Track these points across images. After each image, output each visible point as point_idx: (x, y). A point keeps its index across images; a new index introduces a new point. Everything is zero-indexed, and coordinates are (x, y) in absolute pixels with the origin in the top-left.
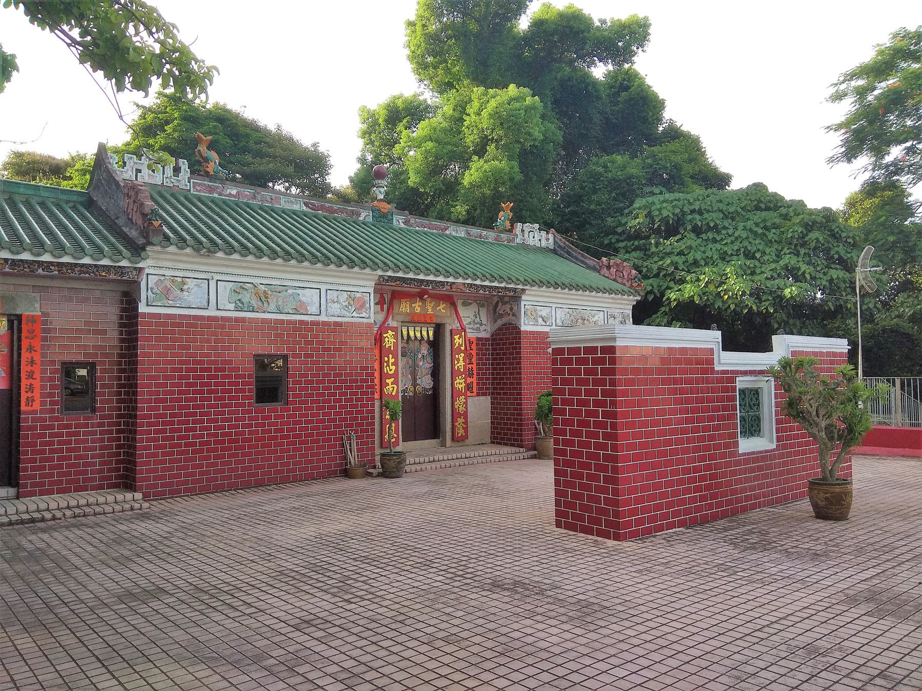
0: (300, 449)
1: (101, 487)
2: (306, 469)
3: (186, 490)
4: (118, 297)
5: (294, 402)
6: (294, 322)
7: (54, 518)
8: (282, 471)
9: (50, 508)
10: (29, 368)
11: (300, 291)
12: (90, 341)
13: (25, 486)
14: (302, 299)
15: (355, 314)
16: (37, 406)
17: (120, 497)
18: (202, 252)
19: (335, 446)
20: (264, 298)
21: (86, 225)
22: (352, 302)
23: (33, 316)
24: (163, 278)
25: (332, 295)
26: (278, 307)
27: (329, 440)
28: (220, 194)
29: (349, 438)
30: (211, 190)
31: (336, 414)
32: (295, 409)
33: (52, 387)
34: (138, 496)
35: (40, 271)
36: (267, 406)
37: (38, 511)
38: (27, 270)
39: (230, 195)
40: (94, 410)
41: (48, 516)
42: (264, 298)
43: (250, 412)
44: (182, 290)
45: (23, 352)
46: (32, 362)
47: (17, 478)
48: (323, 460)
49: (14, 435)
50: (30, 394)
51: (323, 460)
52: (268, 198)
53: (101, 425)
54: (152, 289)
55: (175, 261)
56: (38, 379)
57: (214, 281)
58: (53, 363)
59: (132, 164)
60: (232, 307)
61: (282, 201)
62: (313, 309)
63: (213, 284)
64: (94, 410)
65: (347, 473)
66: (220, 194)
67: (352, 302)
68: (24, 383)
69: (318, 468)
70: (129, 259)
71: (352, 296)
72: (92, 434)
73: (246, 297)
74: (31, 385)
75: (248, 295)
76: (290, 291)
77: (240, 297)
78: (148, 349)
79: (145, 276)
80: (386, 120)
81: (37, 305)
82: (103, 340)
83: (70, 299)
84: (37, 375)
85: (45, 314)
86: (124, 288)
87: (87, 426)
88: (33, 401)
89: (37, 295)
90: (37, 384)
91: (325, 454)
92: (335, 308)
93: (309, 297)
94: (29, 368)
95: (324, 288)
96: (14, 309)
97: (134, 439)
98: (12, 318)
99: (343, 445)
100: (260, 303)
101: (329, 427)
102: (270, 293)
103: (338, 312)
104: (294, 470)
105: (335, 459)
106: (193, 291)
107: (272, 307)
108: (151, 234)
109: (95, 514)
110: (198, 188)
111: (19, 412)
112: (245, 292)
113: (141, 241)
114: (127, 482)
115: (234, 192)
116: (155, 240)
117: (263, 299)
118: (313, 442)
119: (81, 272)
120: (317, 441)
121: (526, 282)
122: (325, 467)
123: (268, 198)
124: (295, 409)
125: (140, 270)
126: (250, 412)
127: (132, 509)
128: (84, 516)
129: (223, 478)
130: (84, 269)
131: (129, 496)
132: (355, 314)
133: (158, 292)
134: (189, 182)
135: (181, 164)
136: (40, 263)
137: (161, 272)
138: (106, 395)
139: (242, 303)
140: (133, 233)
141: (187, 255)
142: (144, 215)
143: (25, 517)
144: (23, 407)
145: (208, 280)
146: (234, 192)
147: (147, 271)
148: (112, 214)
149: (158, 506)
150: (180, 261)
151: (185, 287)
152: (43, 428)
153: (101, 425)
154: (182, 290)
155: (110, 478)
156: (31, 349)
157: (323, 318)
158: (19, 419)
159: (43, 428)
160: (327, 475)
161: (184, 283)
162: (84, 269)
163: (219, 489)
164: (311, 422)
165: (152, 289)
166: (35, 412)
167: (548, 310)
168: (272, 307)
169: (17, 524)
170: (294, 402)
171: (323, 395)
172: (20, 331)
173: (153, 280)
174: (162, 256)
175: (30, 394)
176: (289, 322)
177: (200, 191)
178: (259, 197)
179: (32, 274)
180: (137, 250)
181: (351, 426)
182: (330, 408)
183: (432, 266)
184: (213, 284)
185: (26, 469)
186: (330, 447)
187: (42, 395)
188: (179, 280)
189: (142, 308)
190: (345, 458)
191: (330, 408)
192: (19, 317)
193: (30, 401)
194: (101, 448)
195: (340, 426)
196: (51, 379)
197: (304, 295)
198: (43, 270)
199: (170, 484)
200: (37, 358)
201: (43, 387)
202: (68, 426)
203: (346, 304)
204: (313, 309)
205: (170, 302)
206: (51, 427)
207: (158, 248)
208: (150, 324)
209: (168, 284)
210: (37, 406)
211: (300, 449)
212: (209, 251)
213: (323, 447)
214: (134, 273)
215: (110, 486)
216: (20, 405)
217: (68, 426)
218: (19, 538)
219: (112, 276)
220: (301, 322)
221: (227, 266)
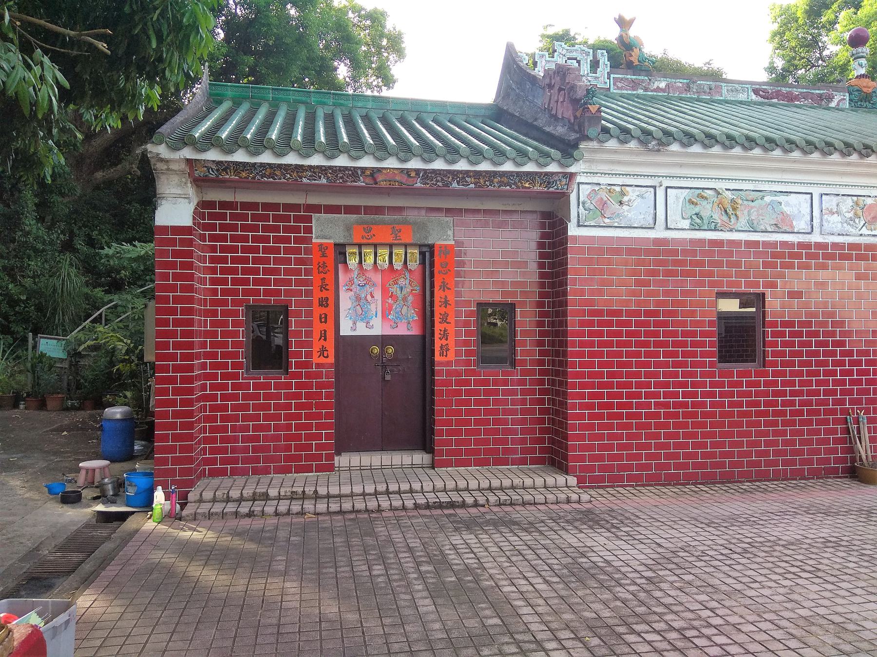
0: (784, 433)
1: (523, 462)
2: (793, 462)
3: (630, 478)
4: (535, 219)
5: (774, 364)
6: (774, 244)
7: (476, 505)
8: (757, 464)
9: (471, 487)
10: (443, 310)
11: (781, 198)
12: (509, 275)
13: (441, 453)
14: (785, 209)
15: (864, 231)
16: (451, 356)
17: (550, 481)
18: (650, 146)
19: (834, 431)
20: (730, 210)
21: (502, 136)
22: (860, 212)
23: (446, 246)
24: (597, 188)
25: (830, 203)
26: (751, 223)
27: (826, 422)
28: (646, 90)
29: (857, 421)
30: (635, 85)
31: (836, 383)
32: (776, 374)
33: (467, 333)
34: (572, 480)
35: (455, 185)
36: (736, 368)
37: (457, 490)
38: (440, 184)
39: (658, 89)
40: (514, 363)
41: (470, 500)
42: (730, 210)
43: (712, 375)
44: (621, 203)
45: (436, 290)
46: (446, 303)
47: (432, 441)
48: (817, 452)
49: (428, 391)
50: (444, 342)
51: (817, 452)
52: (706, 89)
53: (522, 382)
54: (584, 203)
55: (612, 162)
56: (453, 324)
57: (663, 188)
58: (468, 303)
59: (544, 63)
60: (686, 224)
61: (724, 91)
62: (801, 224)
63: (660, 192)
64: (514, 363)
65: (855, 472)
66: (646, 90)
67: (860, 212)
68: (438, 327)
69: (810, 462)
70: (559, 161)
71: (861, 203)
72: (512, 394)
73: (707, 210)
74: (324, 263)
75: (709, 207)
76: (768, 199)
77: (697, 209)
78: (580, 286)
79: (576, 186)
80: (806, 12)
81: (450, 233)
82: (523, 274)
83: (486, 225)
84: (452, 319)
85: (459, 243)
86: (545, 207)
87: (505, 383)
88: (448, 350)
89: (449, 219)
90: (451, 329)
91: (820, 442)
92: (834, 222)
93: (796, 206)
94: (443, 310)
95: (816, 191)
96: (426, 238)
97: (563, 404)
98: (424, 249)
99: (847, 431)
100: (725, 218)
101: (825, 403)
102: (740, 201)
103: (838, 228)
104: (775, 463)
105: (834, 451)
106: (635, 204)
107: (742, 223)
108: (586, 124)
109: (524, 504)
110: (620, 85)
111: (433, 363)
112: (704, 203)
113: (573, 136)
114: (556, 458)
115: (663, 85)
116: (592, 132)
117: (730, 211)
118: (802, 423)
119: (501, 184)
120: (809, 422)
122: (820, 461)
123: (706, 89)
124: (776, 374)
125: (572, 176)
126: (712, 375)
127: (568, 501)
128: (511, 504)
129: (677, 466)
130: (505, 180)
131: (561, 479)
132: (864, 231)
133: (592, 207)
134: (609, 78)
135: (599, 56)
136: (455, 174)
137: (595, 180)
138: (527, 347)
139: (701, 218)
140: (560, 130)
141: (631, 152)
142: (575, 102)
143: (444, 498)
144: (437, 358)
145: (654, 187)
146: (663, 85)
147: (579, 179)
148: (528, 117)
149: (599, 499)
150: (619, 163)
151: (625, 199)
152: (459, 383)
153: (522, 382)
154: (621, 203)
155: (533, 450)
156: (444, 287)
157: (816, 238)
158: (433, 371)
159: (459, 383)
160: (823, 473)
161: (623, 194)
162: (505, 180)
163: (672, 481)
164: (799, 393)
165: (584, 203)
166: (449, 363)
168: (742, 223)
169: (435, 508)
170: (774, 364)
171: (816, 354)
172: (432, 265)
173: (585, 190)
174: (598, 156)
175: (444, 342)
176: (766, 244)
177: (621, 88)
178: (694, 88)
179: (444, 192)
180: (568, 150)
181: (858, 402)
182: (827, 373)
184: (660, 192)
185: (442, 433)
186: (828, 432)
187: (458, 344)
188: (618, 189)
189: (573, 230)
190: (851, 450)
191: (827, 373)
192: (431, 247)
193: (445, 349)
194: (523, 411)
195: (842, 402)
196: (467, 324)
197: (787, 204)
198: (458, 183)
199: (610, 468)
200: (451, 298)
201: (457, 334)
202: (486, 382)
203: (851, 215)
204: (801, 224)
205: (607, 220)
206: (467, 383)
207: (594, 144)
208: (581, 250)
209: (604, 195)
210: (451, 356)
211: (784, 433)
212: (661, 143)
213: (817, 432)
214: (564, 181)
215: (534, 461)
216: (433, 355)
217: (486, 382)
218: (441, 537)
219: (537, 188)
220: (784, 244)
221: (681, 165)
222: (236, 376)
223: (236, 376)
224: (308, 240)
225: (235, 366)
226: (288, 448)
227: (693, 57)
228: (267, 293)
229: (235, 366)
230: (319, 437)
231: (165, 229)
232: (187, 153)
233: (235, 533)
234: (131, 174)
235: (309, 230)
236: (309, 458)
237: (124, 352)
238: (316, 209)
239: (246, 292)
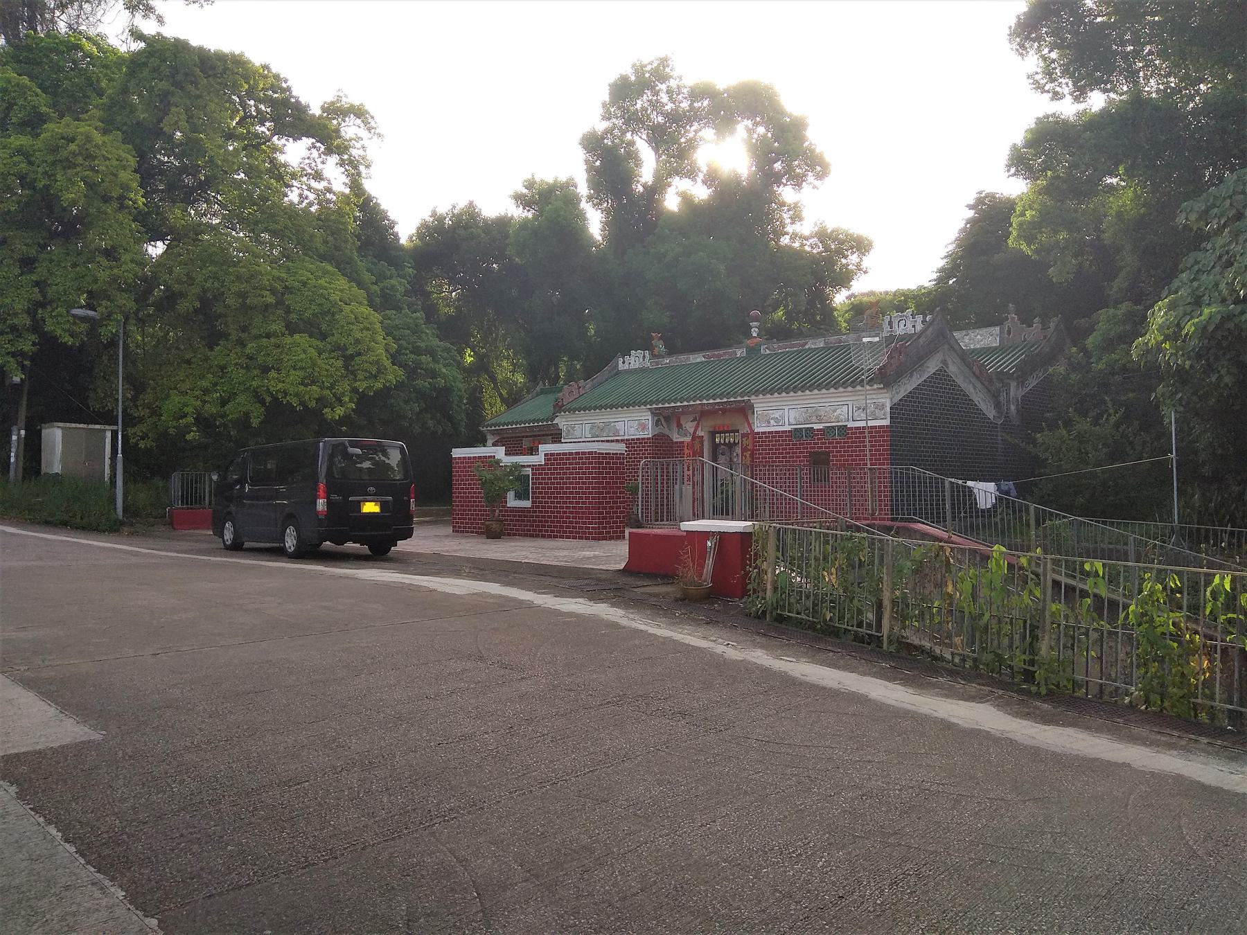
121: (749, 394)
167: (780, 412)
183: (532, 417)
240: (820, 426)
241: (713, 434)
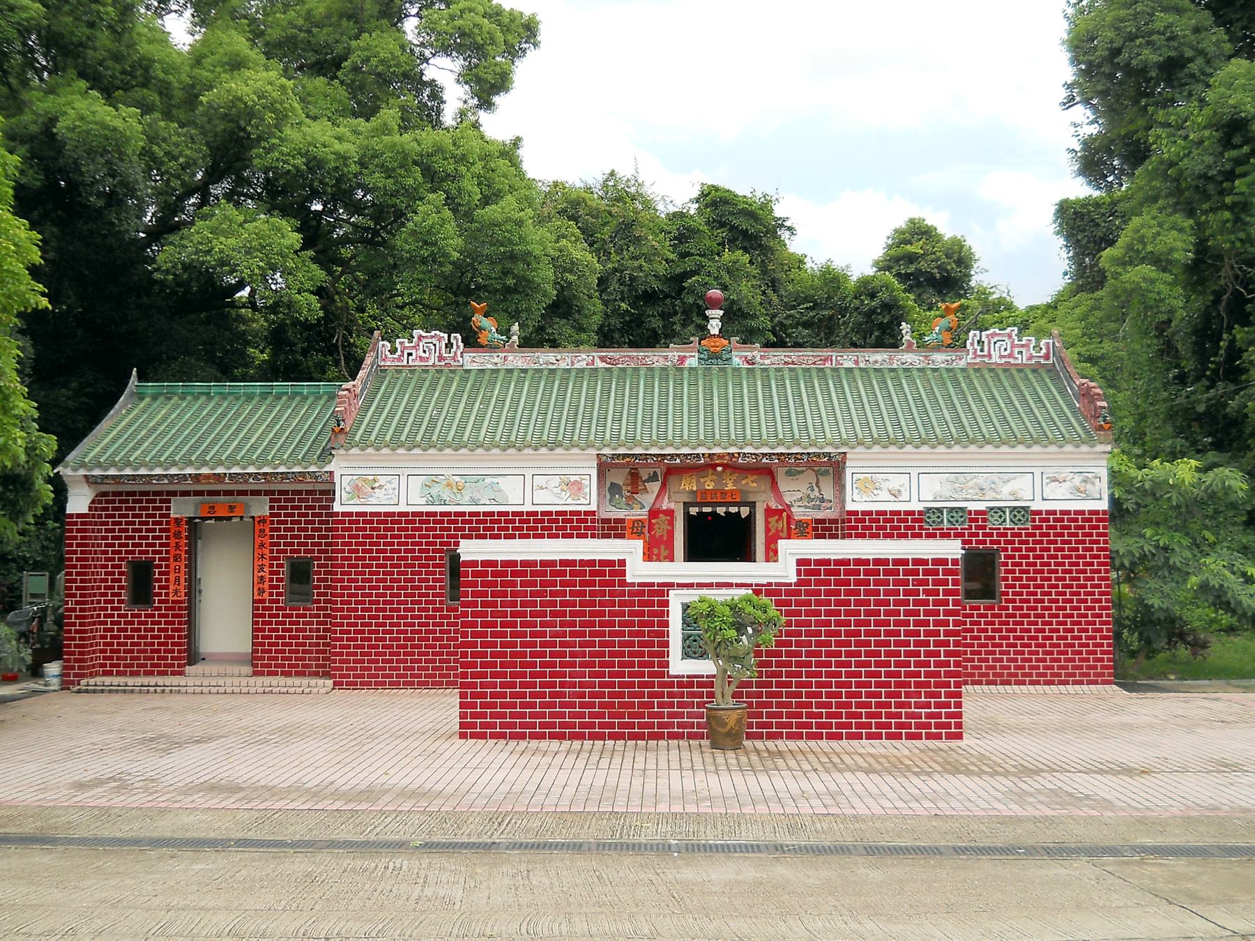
3: (391, 683)
11: (495, 480)
151: (376, 485)
188: (371, 478)
222: (119, 609)
223: (119, 609)
224: (168, 516)
225: (120, 602)
226: (318, 630)
227: (727, 187)
228: (140, 552)
229: (120, 602)
230: (474, 594)
231: (71, 516)
232: (82, 472)
233: (1021, 797)
234: (274, 111)
235: (168, 508)
236: (166, 665)
237: (376, 333)
238: (174, 494)
239: (127, 552)
240: (982, 506)
241: (687, 505)
